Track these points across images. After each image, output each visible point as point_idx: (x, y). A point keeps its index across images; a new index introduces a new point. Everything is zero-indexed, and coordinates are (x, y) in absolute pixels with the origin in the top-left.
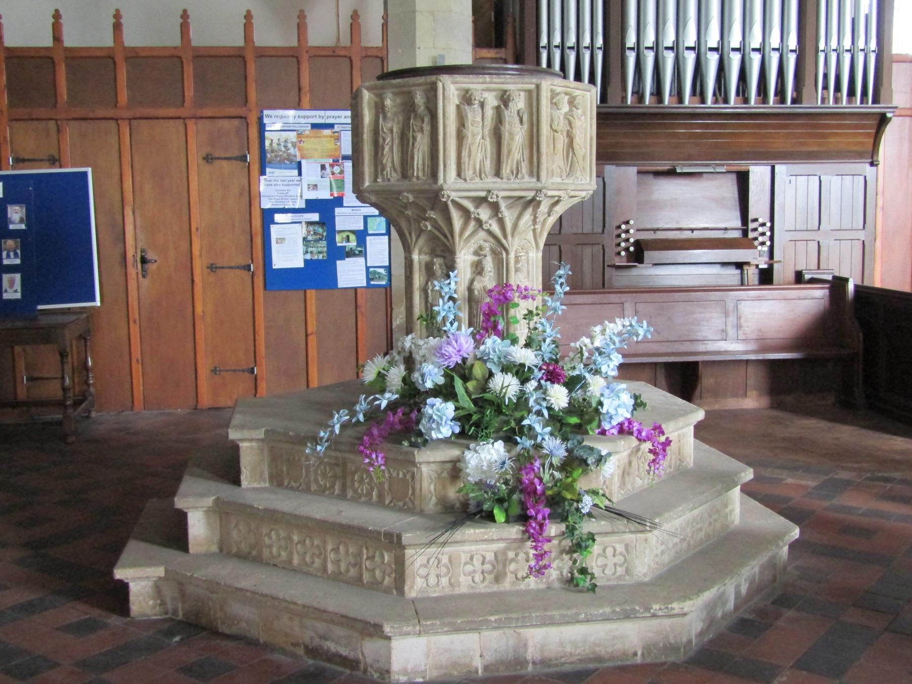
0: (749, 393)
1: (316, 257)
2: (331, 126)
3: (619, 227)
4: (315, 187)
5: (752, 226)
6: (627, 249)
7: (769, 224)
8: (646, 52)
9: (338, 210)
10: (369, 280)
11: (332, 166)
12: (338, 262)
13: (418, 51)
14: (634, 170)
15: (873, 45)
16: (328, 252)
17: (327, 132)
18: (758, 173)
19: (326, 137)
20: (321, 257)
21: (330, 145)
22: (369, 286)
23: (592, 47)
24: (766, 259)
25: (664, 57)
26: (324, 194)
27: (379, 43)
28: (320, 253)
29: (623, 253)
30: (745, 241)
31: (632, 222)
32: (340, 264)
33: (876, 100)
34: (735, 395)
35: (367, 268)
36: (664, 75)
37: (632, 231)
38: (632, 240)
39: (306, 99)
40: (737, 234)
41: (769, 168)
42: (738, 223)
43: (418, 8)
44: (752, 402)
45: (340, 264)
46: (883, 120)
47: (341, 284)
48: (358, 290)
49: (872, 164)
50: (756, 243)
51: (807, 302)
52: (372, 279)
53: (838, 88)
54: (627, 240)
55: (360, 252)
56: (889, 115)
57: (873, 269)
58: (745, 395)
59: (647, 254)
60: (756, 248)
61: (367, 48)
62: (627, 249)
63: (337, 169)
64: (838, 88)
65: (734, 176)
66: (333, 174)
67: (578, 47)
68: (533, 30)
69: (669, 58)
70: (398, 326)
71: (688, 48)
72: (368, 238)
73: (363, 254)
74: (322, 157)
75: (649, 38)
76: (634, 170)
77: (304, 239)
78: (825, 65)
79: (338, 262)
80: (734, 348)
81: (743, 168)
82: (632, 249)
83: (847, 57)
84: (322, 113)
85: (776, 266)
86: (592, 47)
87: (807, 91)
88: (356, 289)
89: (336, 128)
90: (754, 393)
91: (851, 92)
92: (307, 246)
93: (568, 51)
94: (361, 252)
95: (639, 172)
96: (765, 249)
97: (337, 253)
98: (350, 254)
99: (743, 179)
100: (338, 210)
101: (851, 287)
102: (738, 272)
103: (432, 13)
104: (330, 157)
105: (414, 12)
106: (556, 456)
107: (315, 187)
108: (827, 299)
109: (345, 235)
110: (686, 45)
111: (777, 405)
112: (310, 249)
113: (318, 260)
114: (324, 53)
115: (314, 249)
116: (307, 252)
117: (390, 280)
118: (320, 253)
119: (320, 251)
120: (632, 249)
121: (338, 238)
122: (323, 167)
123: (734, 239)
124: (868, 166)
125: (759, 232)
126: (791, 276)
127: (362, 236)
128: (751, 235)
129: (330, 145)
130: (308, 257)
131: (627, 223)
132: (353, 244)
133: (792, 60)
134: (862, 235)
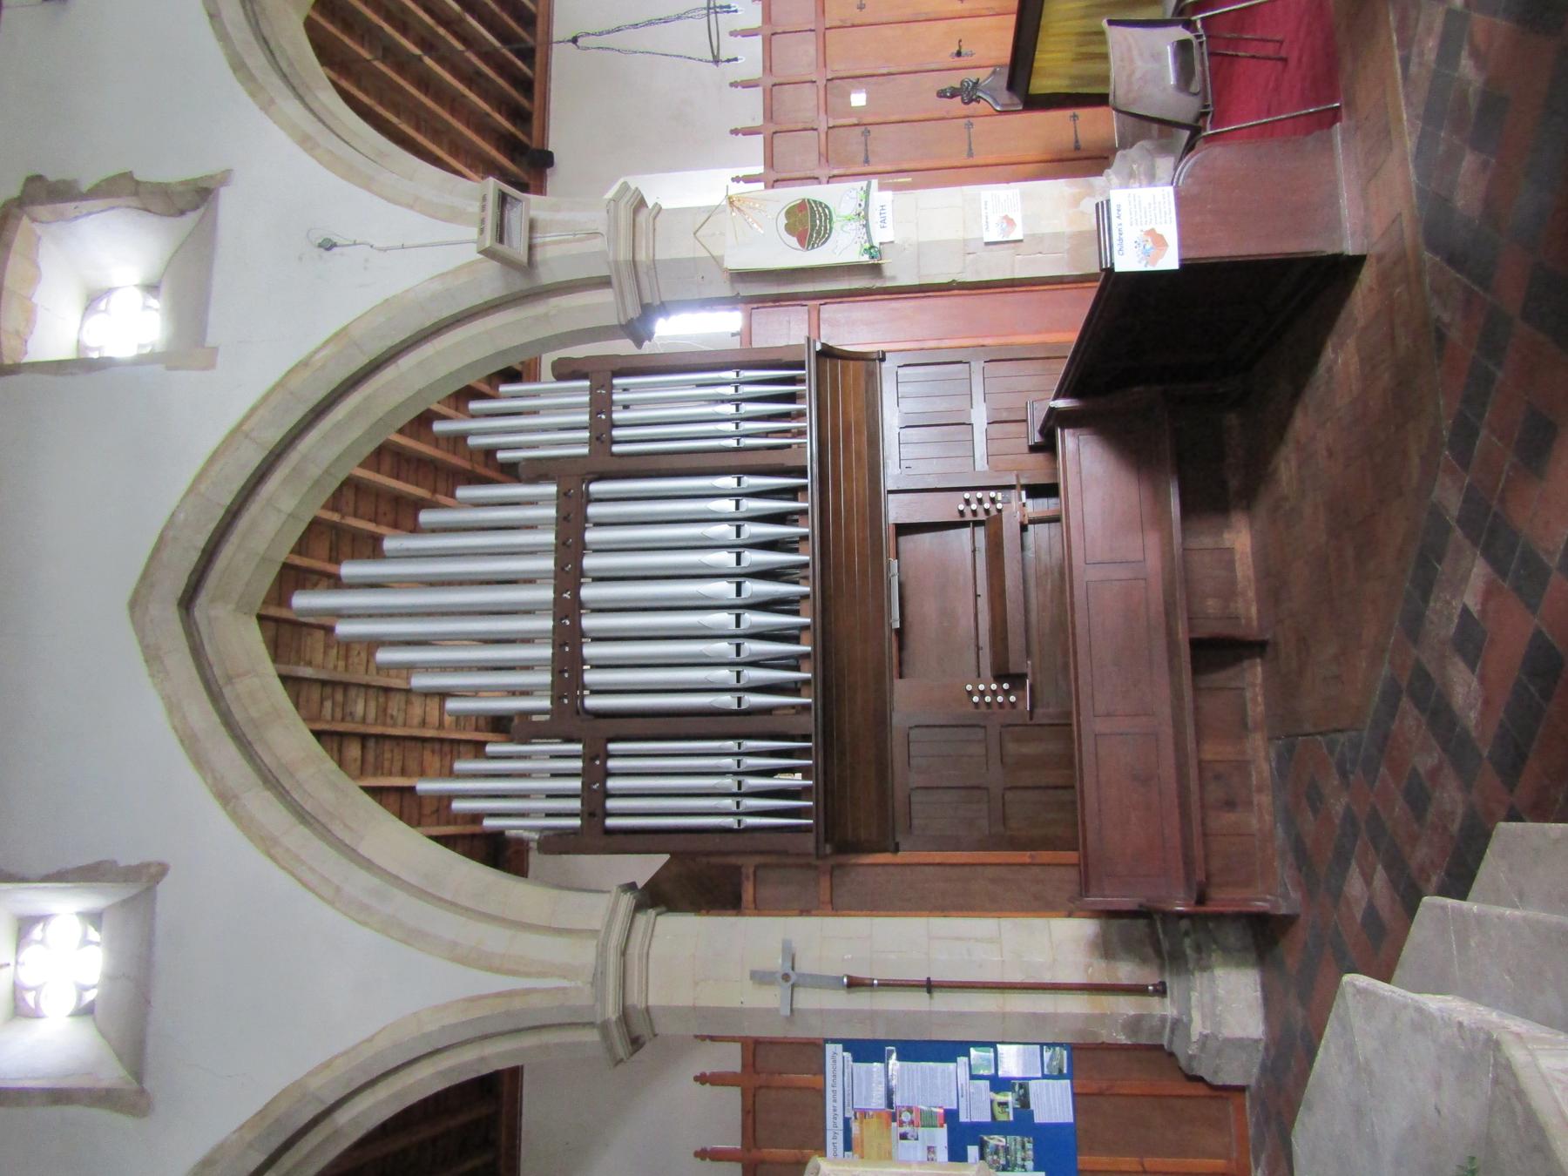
0: (1228, 545)
1: (1030, 1153)
2: (847, 1121)
3: (976, 704)
4: (930, 1149)
5: (969, 517)
6: (1007, 693)
7: (967, 495)
8: (743, 626)
9: (963, 1118)
10: (1060, 1076)
11: (901, 1124)
12: (1037, 1119)
13: (747, 1005)
14: (898, 683)
15: (730, 375)
16: (1023, 1134)
17: (855, 1127)
18: (897, 510)
19: (861, 1129)
20: (1029, 1146)
21: (873, 1125)
22: (1070, 1076)
23: (737, 496)
24: (1014, 493)
25: (751, 655)
26: (941, 1136)
27: (736, 1048)
28: (1023, 1147)
29: (1012, 699)
30: (992, 525)
31: (969, 687)
32: (1039, 1118)
33: (800, 366)
34: (1230, 565)
35: (1044, 1077)
36: (767, 594)
37: (982, 687)
38: (994, 686)
39: (806, 1078)
40: (980, 532)
41: (891, 496)
42: (967, 531)
43: (690, 1003)
44: (1240, 539)
45: (1039, 1118)
46: (827, 353)
47: (1071, 1120)
48: (1078, 1090)
49: (883, 360)
50: (993, 513)
51: (1085, 463)
52: (1060, 1071)
53: (785, 416)
54: (994, 694)
55: (1021, 1086)
56: (819, 347)
57: (1024, 345)
58: (1231, 550)
59: (1013, 669)
60: (999, 511)
61: (744, 1066)
62: (1007, 693)
63: (906, 1117)
64: (785, 416)
65: (902, 539)
66: (912, 1123)
67: (737, 401)
68: (717, 838)
69: (753, 647)
70: (1128, 1037)
71: (737, 507)
72: (1001, 1074)
73: (1023, 1083)
74: (889, 1137)
75: (724, 675)
76: (898, 683)
77: (1004, 1169)
78: (756, 433)
79: (1037, 1119)
80: (1146, 553)
81: (892, 531)
82: (1006, 686)
83: (747, 408)
84: (829, 1135)
85: (1023, 481)
86: (737, 496)
87: (788, 460)
88: (1075, 1095)
89: (849, 1114)
90: (1226, 536)
91: (791, 398)
92: (1016, 1165)
93: (742, 768)
94: (1020, 1087)
95: (901, 676)
96: (1000, 496)
97: (1023, 1122)
98: (1024, 1101)
99: (904, 529)
100: (963, 1118)
101: (1061, 404)
102: (1031, 527)
103: (696, 984)
104: (889, 1126)
105: (694, 1008)
106: (1180, 581)
107: (930, 1149)
108: (1078, 431)
109: (997, 1109)
110: (734, 564)
111: (1247, 498)
112: (1019, 1162)
113: (1035, 1150)
114: (750, 1121)
115: (1020, 1155)
116: (1023, 1166)
117: (1060, 1045)
118: (1023, 1147)
119: (1022, 1147)
120: (1006, 686)
121: (1001, 1118)
122: (904, 1137)
123: (988, 536)
124: (884, 365)
125: (977, 504)
126: (1040, 457)
127: (999, 1084)
128: (982, 516)
129: (873, 1125)
130: (1029, 1164)
131: (970, 694)
132: (1009, 1097)
133: (751, 482)
134: (977, 366)
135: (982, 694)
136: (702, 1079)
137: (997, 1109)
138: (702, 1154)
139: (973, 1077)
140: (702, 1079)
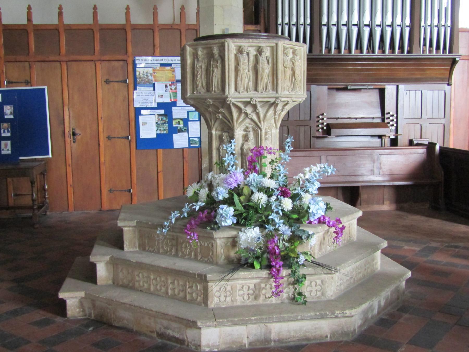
0: (385, 202)
1: (162, 132)
2: (170, 65)
3: (318, 117)
4: (162, 96)
5: (386, 116)
6: (322, 128)
7: (395, 115)
8: (332, 27)
9: (174, 108)
10: (190, 144)
11: (171, 85)
12: (174, 135)
13: (215, 26)
14: (326, 87)
15: (449, 23)
16: (169, 130)
17: (168, 68)
18: (390, 89)
19: (168, 70)
20: (165, 132)
21: (170, 75)
22: (190, 147)
23: (304, 24)
24: (394, 133)
25: (341, 30)
26: (167, 100)
27: (195, 22)
28: (164, 130)
29: (320, 130)
30: (383, 124)
31: (325, 114)
32: (175, 136)
33: (450, 52)
34: (378, 203)
35: (189, 138)
36: (342, 38)
37: (325, 119)
38: (325, 124)
39: (157, 51)
40: (379, 121)
41: (395, 87)
42: (379, 115)
43: (215, 4)
44: (387, 207)
45: (175, 136)
46: (454, 62)
47: (175, 146)
48: (184, 149)
49: (448, 84)
50: (389, 125)
51: (415, 155)
52: (191, 144)
53: (431, 45)
54: (322, 124)
55: (185, 129)
56: (457, 59)
57: (449, 139)
58: (383, 203)
59: (333, 131)
60: (389, 127)
61: (189, 25)
62: (322, 128)
63: (173, 87)
64: (431, 45)
65: (377, 91)
66: (171, 89)
67: (297, 24)
68: (274, 15)
69: (344, 30)
70: (205, 168)
71: (354, 25)
72: (189, 123)
73: (187, 131)
74: (165, 81)
75: (334, 20)
76: (326, 87)
78: (424, 33)
79: (174, 135)
80: (377, 179)
81: (382, 87)
82: (325, 128)
83: (436, 30)
84: (165, 58)
85: (399, 137)
86: (304, 24)
87: (415, 47)
88: (183, 149)
89: (173, 66)
90: (388, 202)
91: (438, 48)
92: (158, 127)
93: (292, 26)
94: (186, 129)
95: (329, 89)
96: (394, 128)
97: (173, 130)
98: (180, 131)
99: (382, 92)
100: (174, 108)
101: (437, 148)
102: (380, 140)
103: (222, 7)
104: (170, 81)
105: (213, 6)
107: (162, 96)
108: (425, 154)
109: (177, 121)
110: (353, 23)
111: (400, 209)
112: (159, 128)
113: (163, 134)
114: (166, 27)
116: (158, 130)
117: (200, 144)
118: (164, 130)
119: (164, 129)
120: (325, 128)
121: (174, 122)
122: (166, 86)
123: (378, 123)
124: (446, 85)
125: (390, 119)
126: (407, 142)
127: (186, 121)
128: (386, 121)
129: (170, 75)
130: (159, 132)
131: (323, 115)
132: (181, 125)
133: (407, 31)
134: (443, 121)
135: (322, 119)
136: (128, 8)
137: (177, 121)
138: (95, 8)
139: (188, 112)
140: (128, 8)
